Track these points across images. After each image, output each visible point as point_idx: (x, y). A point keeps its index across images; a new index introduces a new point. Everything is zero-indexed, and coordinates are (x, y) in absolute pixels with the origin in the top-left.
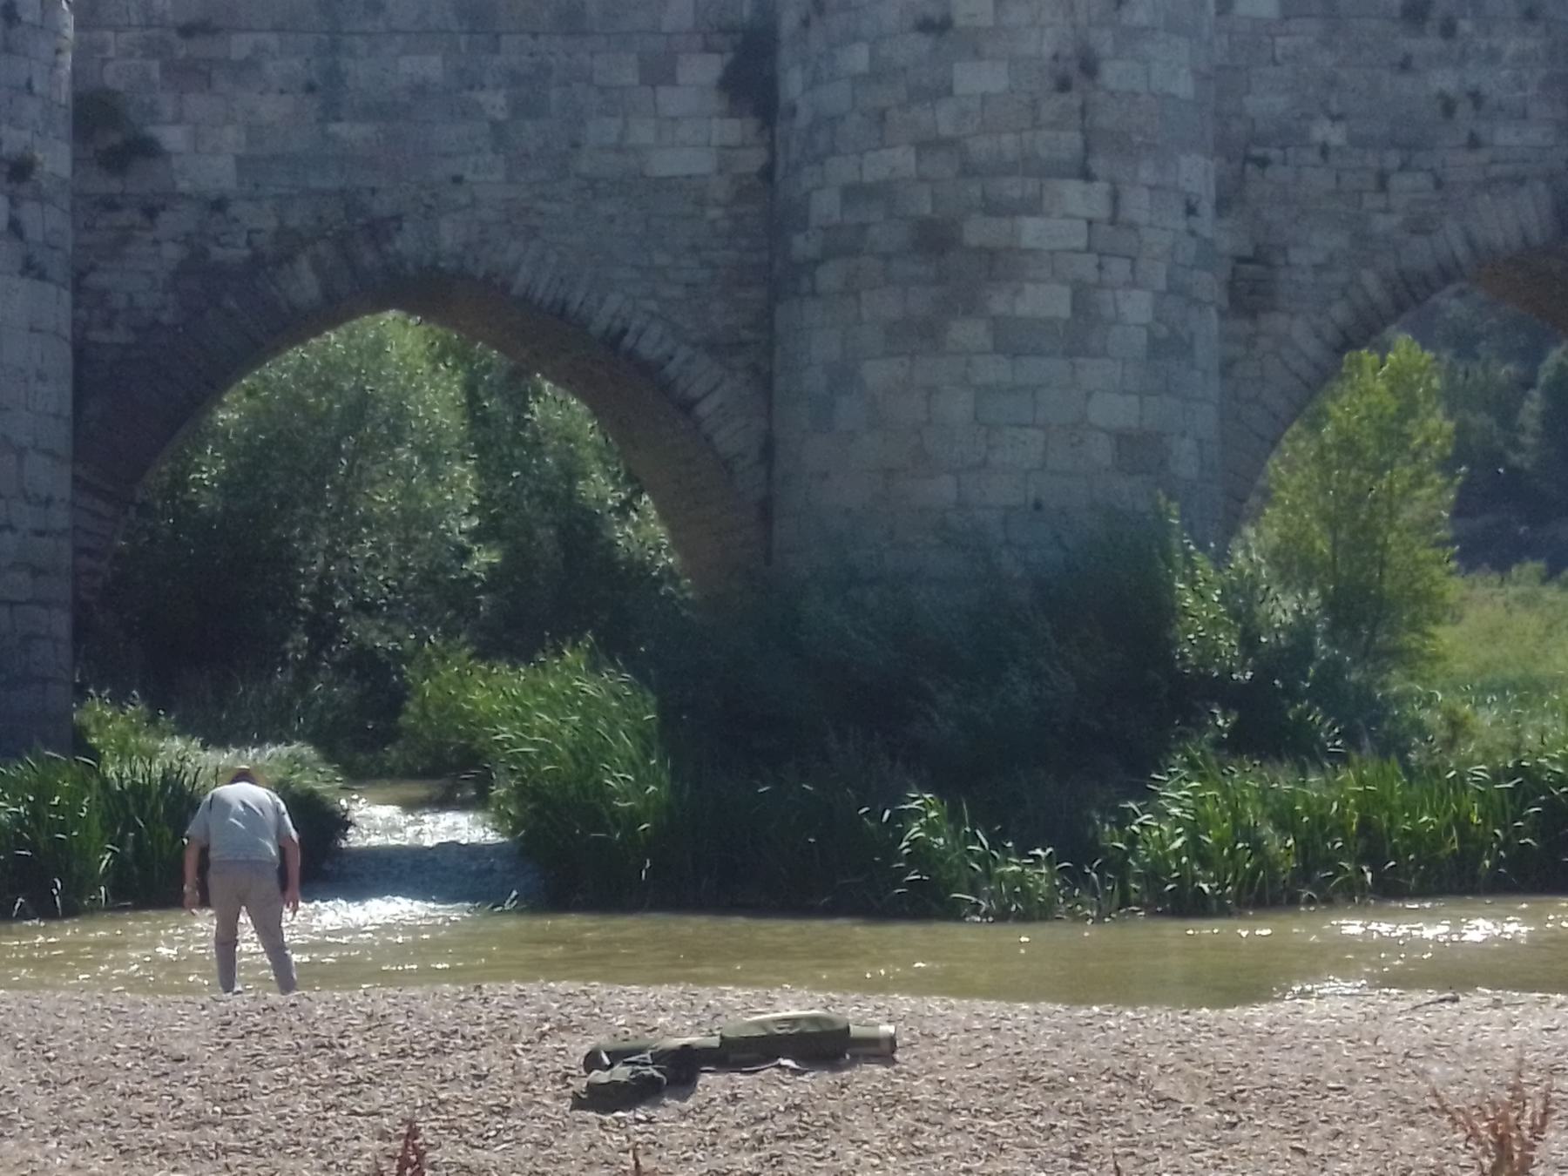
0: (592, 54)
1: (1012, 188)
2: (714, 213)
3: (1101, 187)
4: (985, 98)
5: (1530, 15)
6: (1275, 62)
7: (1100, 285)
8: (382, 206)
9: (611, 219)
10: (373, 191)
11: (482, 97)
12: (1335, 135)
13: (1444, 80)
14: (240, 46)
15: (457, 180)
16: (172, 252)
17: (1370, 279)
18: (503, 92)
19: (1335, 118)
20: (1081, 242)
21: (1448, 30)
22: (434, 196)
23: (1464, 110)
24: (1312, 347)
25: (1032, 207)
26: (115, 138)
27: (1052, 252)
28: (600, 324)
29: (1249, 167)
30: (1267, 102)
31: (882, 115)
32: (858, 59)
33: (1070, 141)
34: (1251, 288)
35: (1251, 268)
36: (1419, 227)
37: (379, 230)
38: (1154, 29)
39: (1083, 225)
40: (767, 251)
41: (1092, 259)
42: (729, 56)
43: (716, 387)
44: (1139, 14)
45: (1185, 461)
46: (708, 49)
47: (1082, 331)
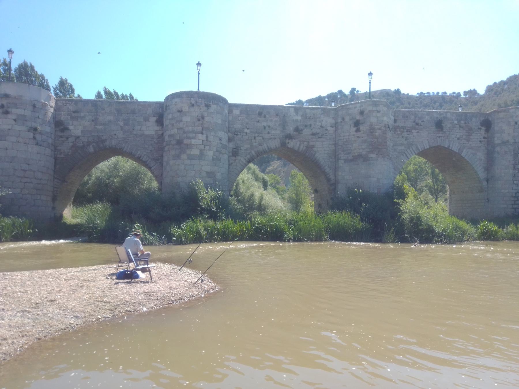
1: (191, 135)
2: (154, 140)
7: (204, 150)
8: (104, 138)
11: (119, 122)
13: (264, 124)
14: (82, 114)
15: (115, 134)
16: (71, 144)
17: (253, 152)
19: (248, 129)
20: (201, 143)
21: (265, 117)
23: (267, 128)
24: (244, 161)
25: (194, 138)
26: (62, 127)
28: (137, 155)
30: (238, 126)
31: (173, 125)
32: (170, 116)
34: (235, 153)
37: (103, 141)
40: (160, 144)
41: (203, 146)
45: (219, 176)
46: (154, 116)
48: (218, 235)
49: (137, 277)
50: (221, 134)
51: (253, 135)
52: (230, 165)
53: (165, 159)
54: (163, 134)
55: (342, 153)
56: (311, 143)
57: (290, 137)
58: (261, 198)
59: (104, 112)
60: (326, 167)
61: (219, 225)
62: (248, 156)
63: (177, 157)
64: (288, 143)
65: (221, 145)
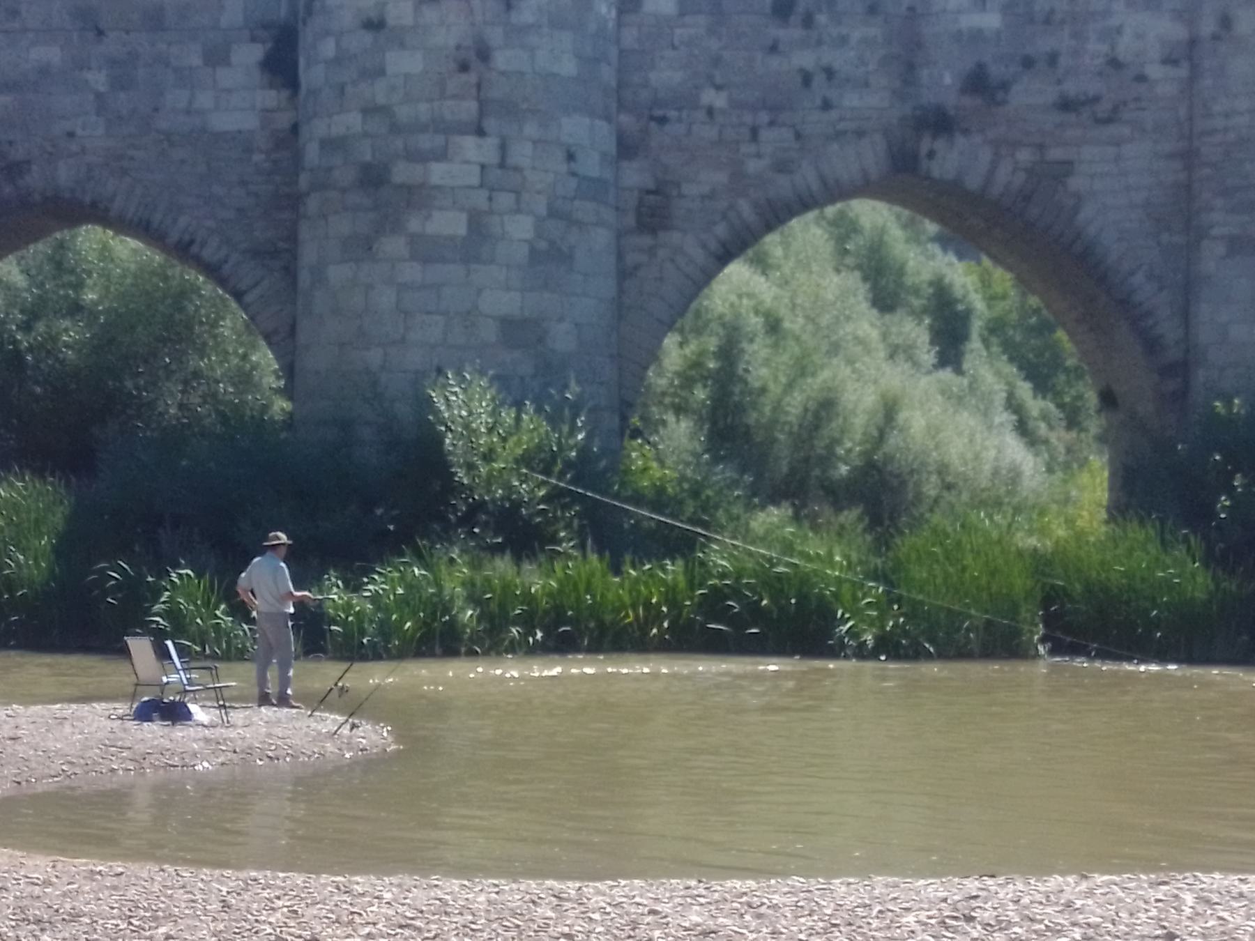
0: (170, 44)
1: (425, 142)
2: (258, 157)
3: (491, 142)
4: (407, 76)
5: (872, 10)
6: (674, 47)
7: (491, 212)
8: (18, 154)
9: (183, 162)
10: (10, 143)
12: (719, 100)
13: (806, 59)
15: (71, 135)
18: (104, 72)
19: (719, 88)
20: (475, 180)
21: (808, 22)
22: (54, 146)
23: (819, 80)
24: (699, 255)
25: (442, 155)
27: (453, 188)
29: (653, 124)
30: (666, 75)
31: (342, 90)
32: (328, 48)
33: (468, 109)
35: (652, 197)
36: (782, 167)
38: (540, 27)
39: (477, 169)
41: (484, 193)
42: (269, 45)
43: (256, 284)
44: (525, 15)
45: (562, 339)
46: (253, 39)
47: (477, 242)
48: (528, 623)
49: (188, 716)
50: (575, 128)
51: (748, 118)
52: (624, 274)
53: (308, 254)
54: (295, 129)
55: (1219, 202)
56: (1055, 154)
57: (940, 123)
58: (889, 410)
59: (17, 25)
60: (1139, 278)
61: (536, 581)
62: (721, 230)
63: (361, 248)
64: (931, 155)
65: (573, 183)
